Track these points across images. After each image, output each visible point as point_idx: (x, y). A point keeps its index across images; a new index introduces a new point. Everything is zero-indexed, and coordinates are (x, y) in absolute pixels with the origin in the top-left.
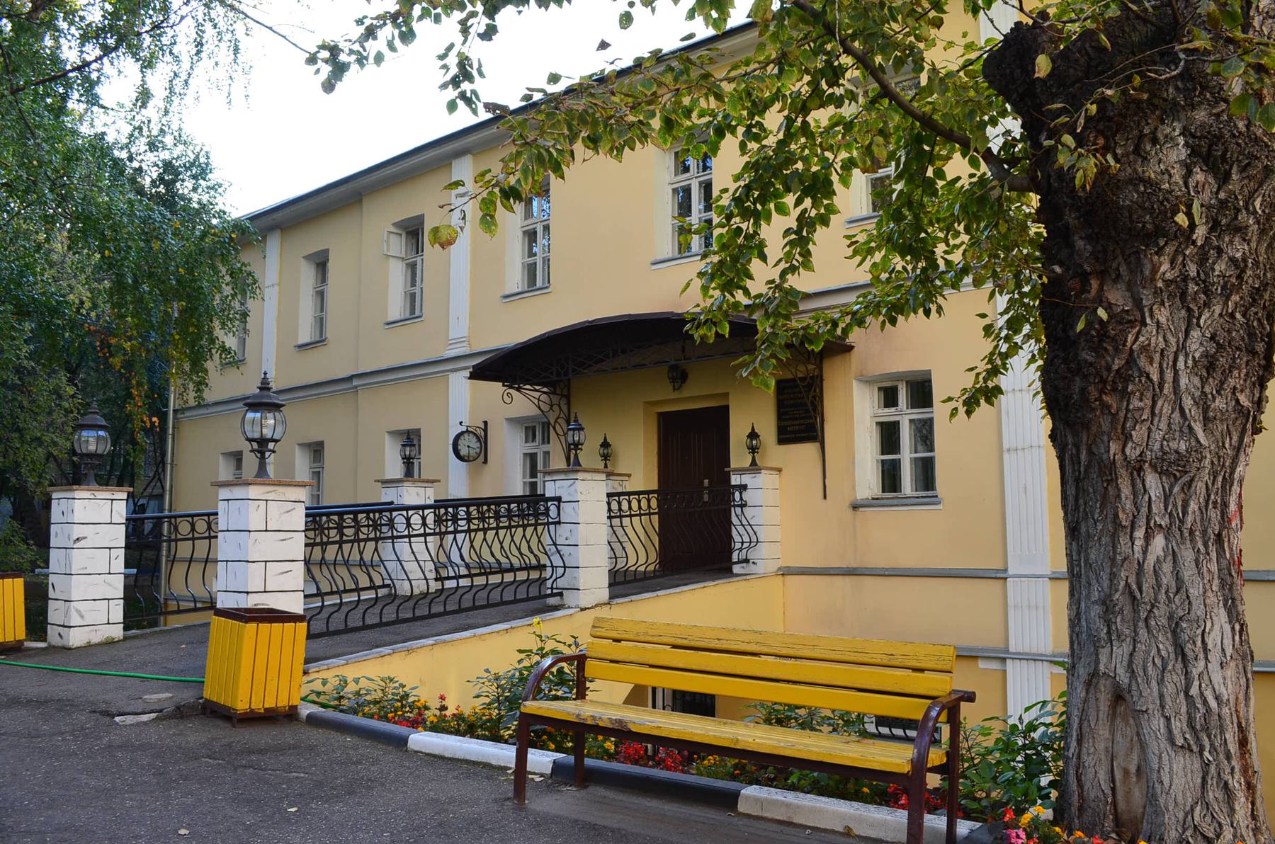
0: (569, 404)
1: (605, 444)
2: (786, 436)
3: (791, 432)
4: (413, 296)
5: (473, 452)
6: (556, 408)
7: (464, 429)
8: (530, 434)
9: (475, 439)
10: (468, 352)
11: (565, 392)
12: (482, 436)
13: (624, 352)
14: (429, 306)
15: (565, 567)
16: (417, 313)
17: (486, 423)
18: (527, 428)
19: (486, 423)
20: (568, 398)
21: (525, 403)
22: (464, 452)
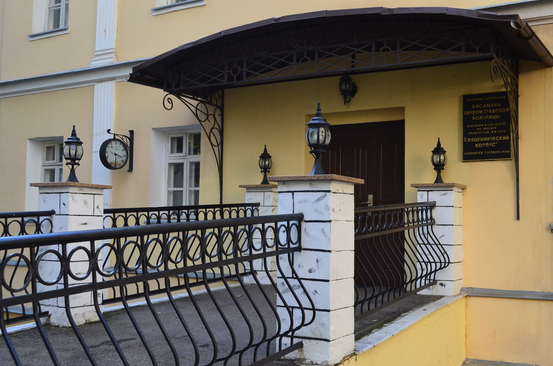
0: (222, 116)
1: (265, 156)
2: (471, 153)
3: (479, 149)
4: (57, 13)
5: (119, 160)
6: (211, 118)
7: (112, 137)
8: (178, 144)
9: (121, 148)
10: (115, 63)
11: (219, 104)
12: (129, 144)
13: (321, 55)
14: (74, 20)
15: (314, 310)
16: (62, 26)
17: (132, 132)
18: (172, 139)
19: (132, 132)
20: (222, 108)
21: (181, 112)
22: (111, 159)
